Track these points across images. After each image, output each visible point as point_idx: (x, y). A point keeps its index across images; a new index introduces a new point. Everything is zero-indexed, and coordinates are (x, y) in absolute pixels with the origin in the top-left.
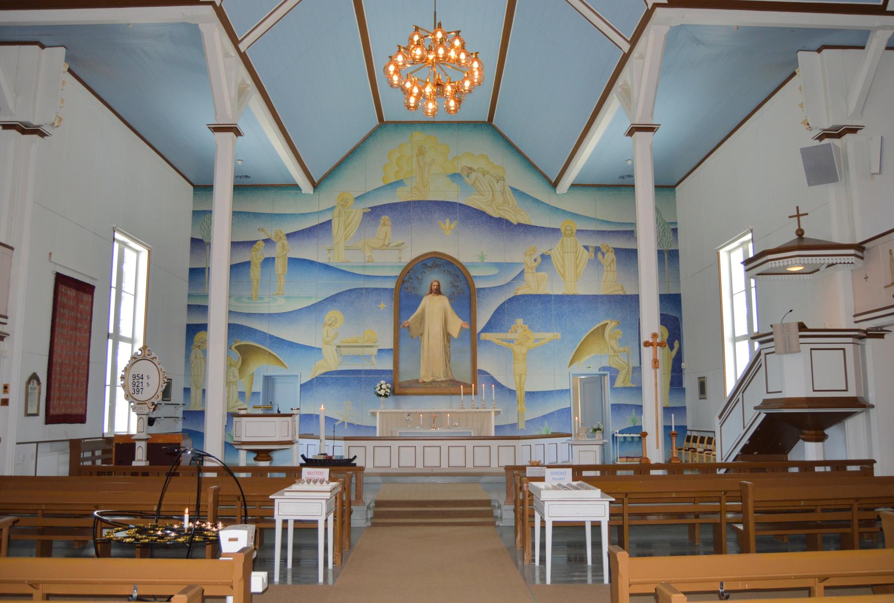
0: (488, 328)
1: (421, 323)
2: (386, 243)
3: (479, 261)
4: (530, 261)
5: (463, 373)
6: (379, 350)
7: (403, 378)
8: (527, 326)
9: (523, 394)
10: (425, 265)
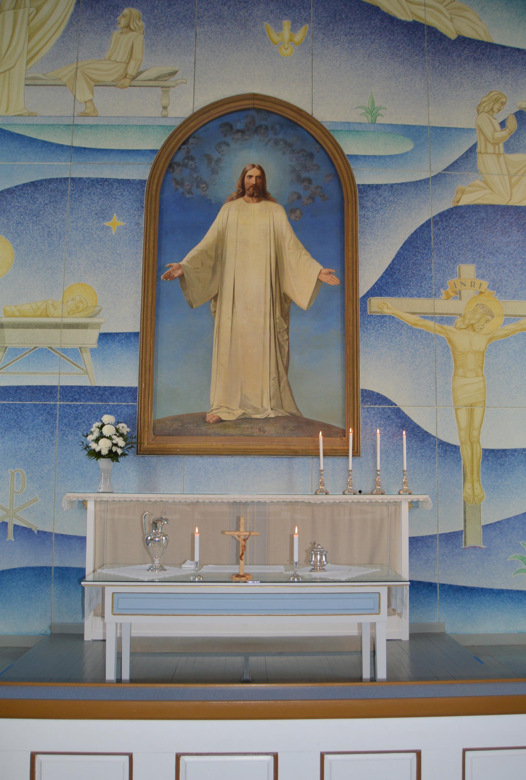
0: (391, 283)
1: (214, 269)
2: (132, 70)
3: (365, 120)
4: (489, 126)
5: (320, 396)
6: (104, 337)
7: (167, 407)
8: (485, 284)
9: (479, 454)
10: (228, 128)
